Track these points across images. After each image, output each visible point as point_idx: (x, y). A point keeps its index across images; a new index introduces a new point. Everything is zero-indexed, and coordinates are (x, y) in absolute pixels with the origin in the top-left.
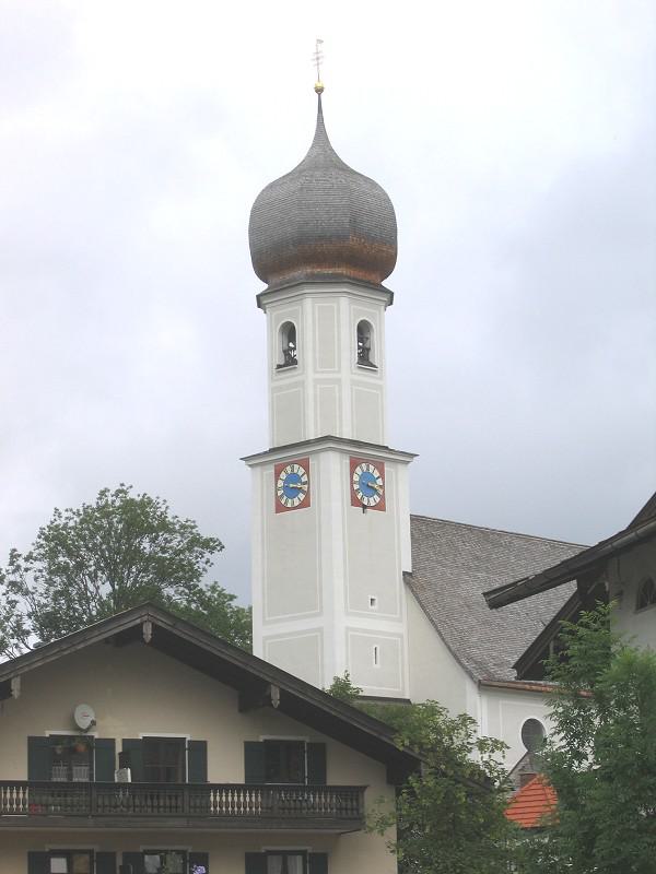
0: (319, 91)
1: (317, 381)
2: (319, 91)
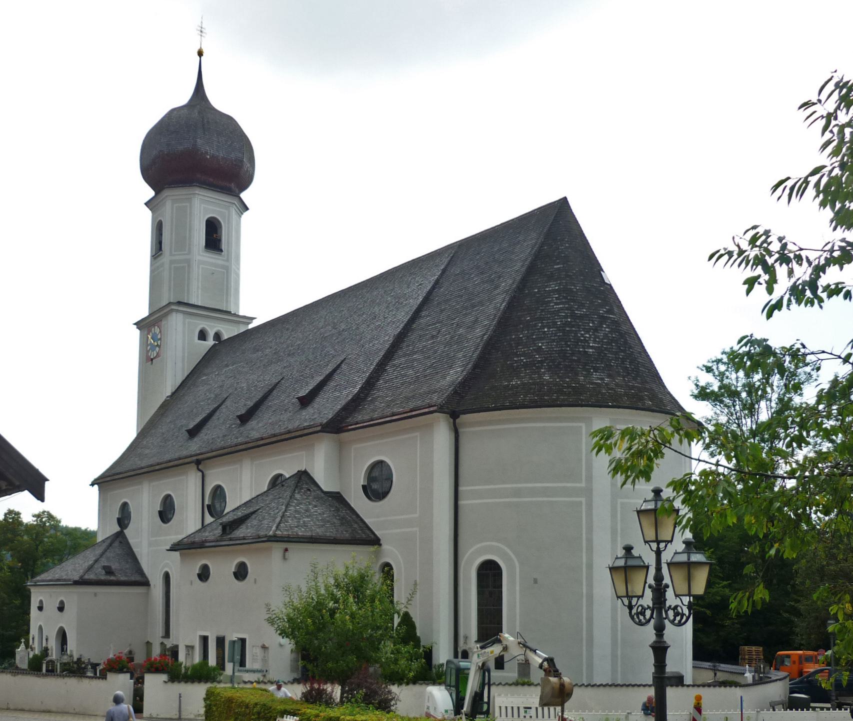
0: (200, 54)
1: (171, 262)
2: (200, 54)
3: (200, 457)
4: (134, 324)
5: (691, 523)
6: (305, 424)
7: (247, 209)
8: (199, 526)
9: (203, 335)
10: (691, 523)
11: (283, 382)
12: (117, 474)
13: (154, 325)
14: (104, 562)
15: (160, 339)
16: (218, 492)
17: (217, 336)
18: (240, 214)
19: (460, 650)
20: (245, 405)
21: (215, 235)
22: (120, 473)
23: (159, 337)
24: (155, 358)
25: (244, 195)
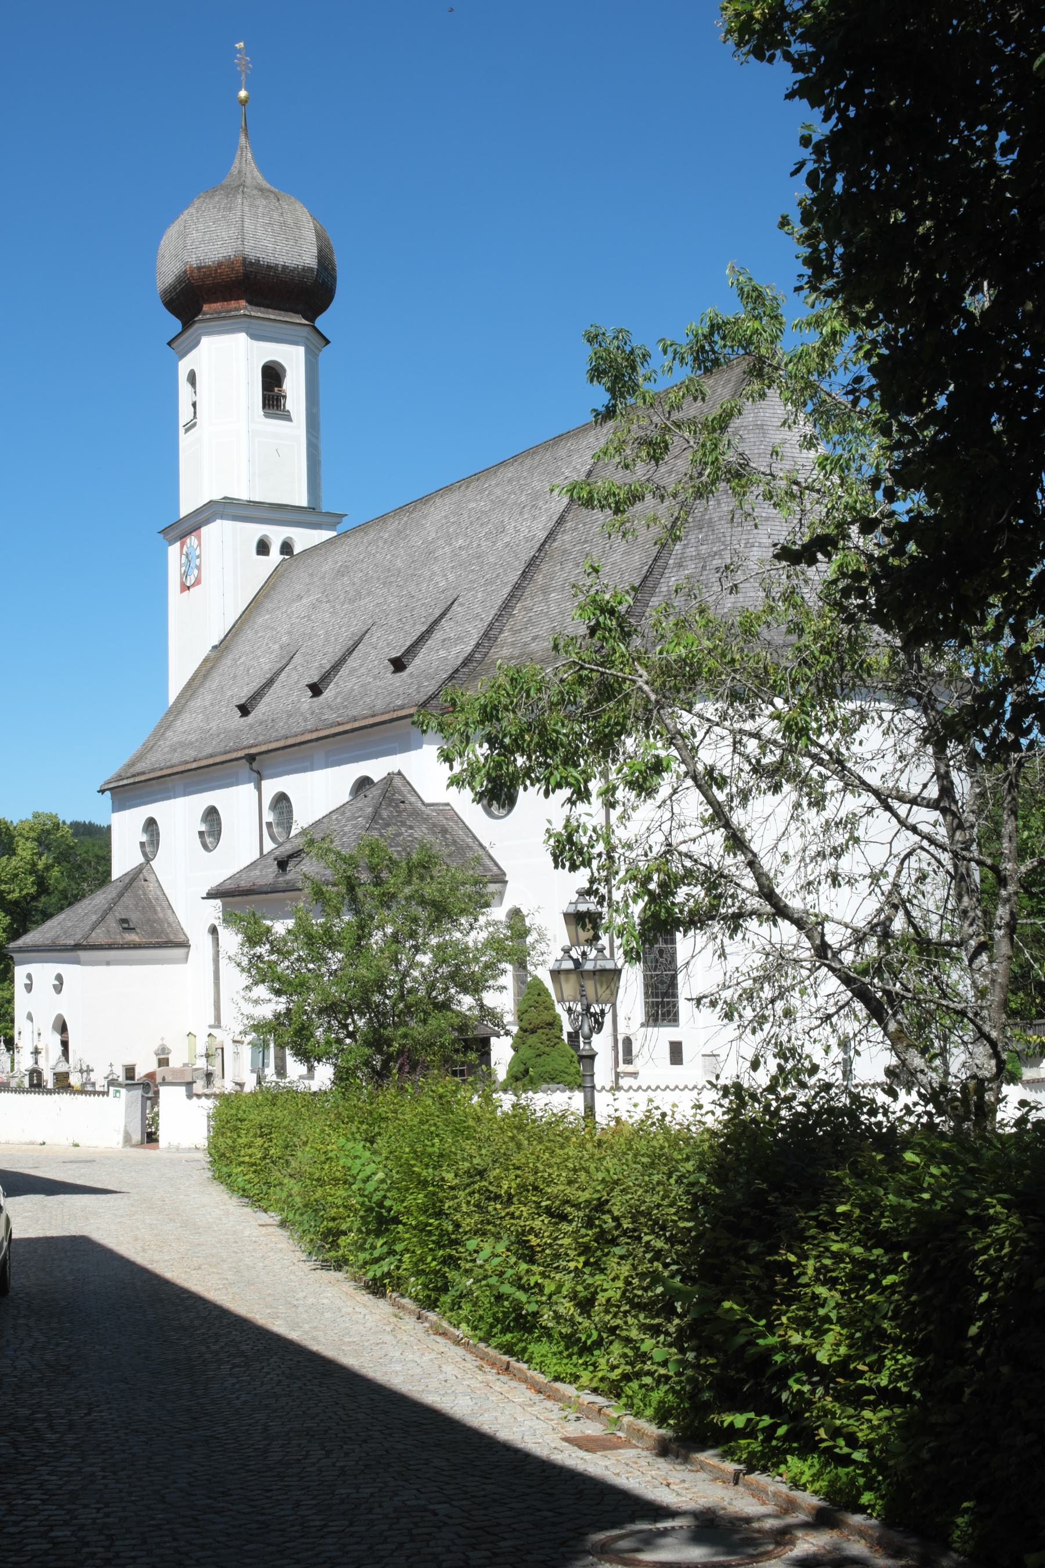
3: (253, 751)
4: (790, 96)
5: (924, 400)
6: (399, 702)
7: (327, 342)
8: (258, 856)
9: (263, 548)
10: (924, 400)
11: (374, 628)
12: (139, 774)
13: (190, 533)
14: (119, 912)
15: (199, 557)
16: (282, 801)
17: (286, 548)
18: (316, 351)
19: (620, 1038)
20: (321, 666)
21: (276, 389)
22: (143, 773)
23: (197, 553)
24: (193, 585)
25: (321, 322)
